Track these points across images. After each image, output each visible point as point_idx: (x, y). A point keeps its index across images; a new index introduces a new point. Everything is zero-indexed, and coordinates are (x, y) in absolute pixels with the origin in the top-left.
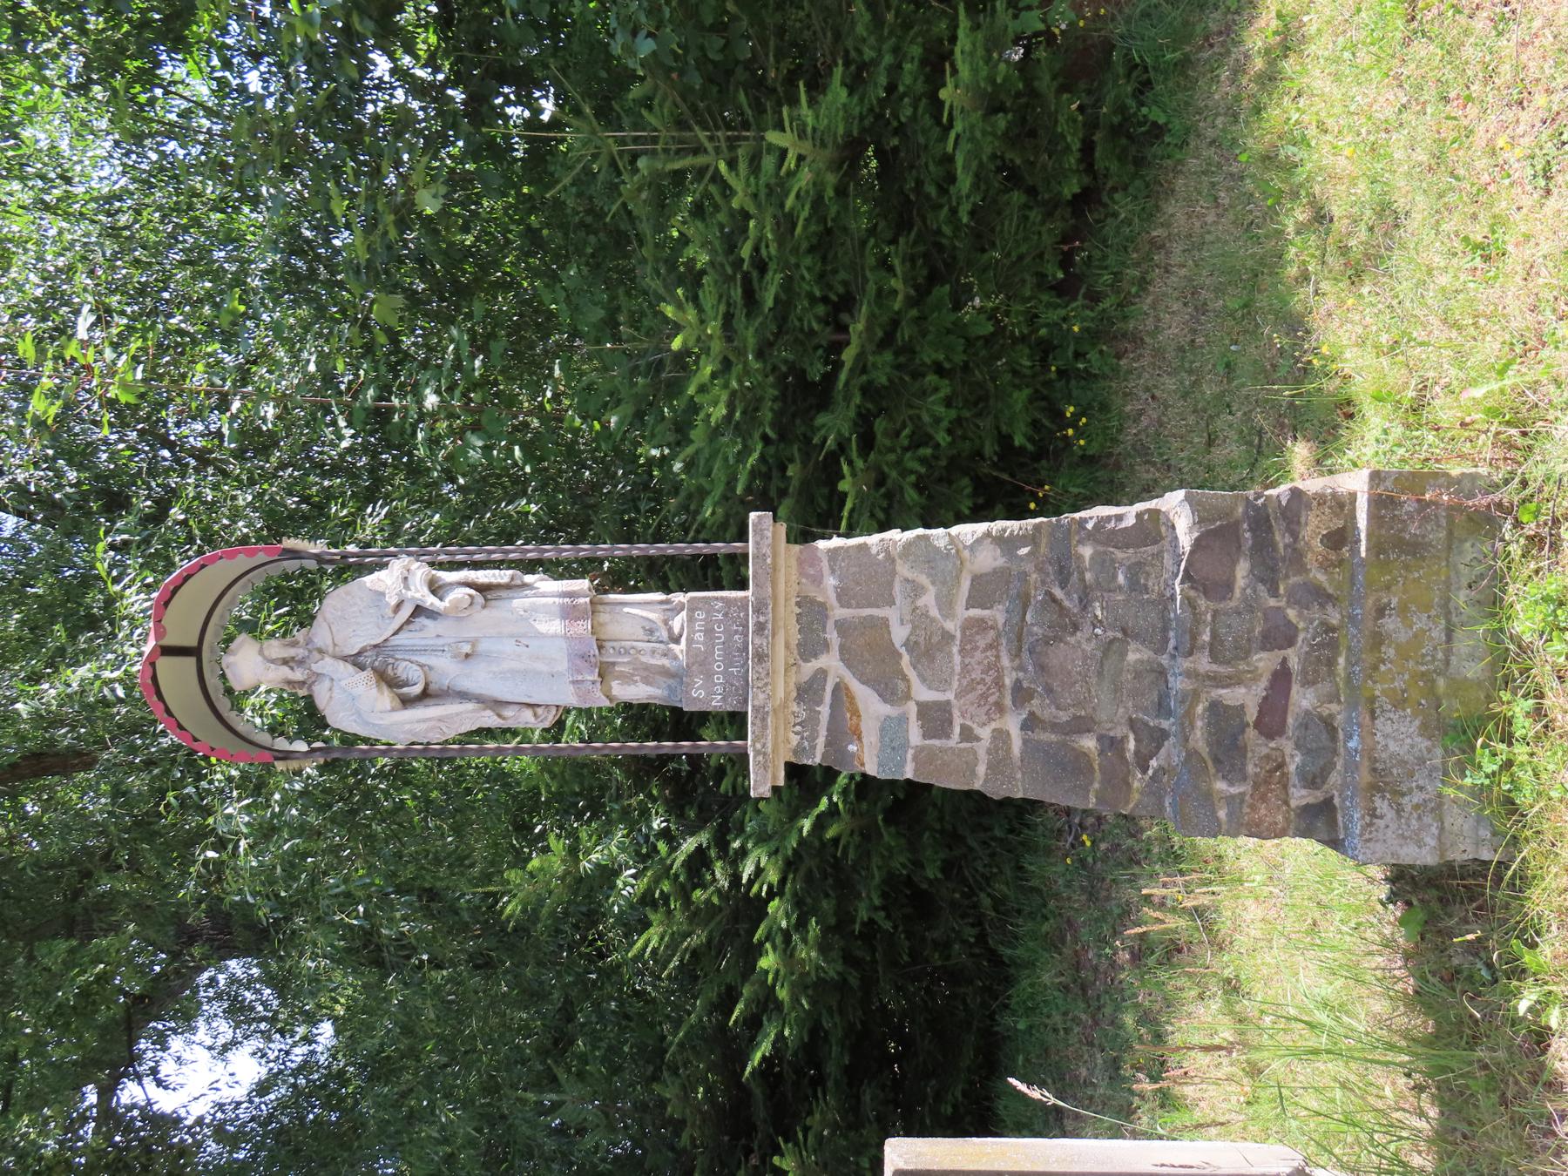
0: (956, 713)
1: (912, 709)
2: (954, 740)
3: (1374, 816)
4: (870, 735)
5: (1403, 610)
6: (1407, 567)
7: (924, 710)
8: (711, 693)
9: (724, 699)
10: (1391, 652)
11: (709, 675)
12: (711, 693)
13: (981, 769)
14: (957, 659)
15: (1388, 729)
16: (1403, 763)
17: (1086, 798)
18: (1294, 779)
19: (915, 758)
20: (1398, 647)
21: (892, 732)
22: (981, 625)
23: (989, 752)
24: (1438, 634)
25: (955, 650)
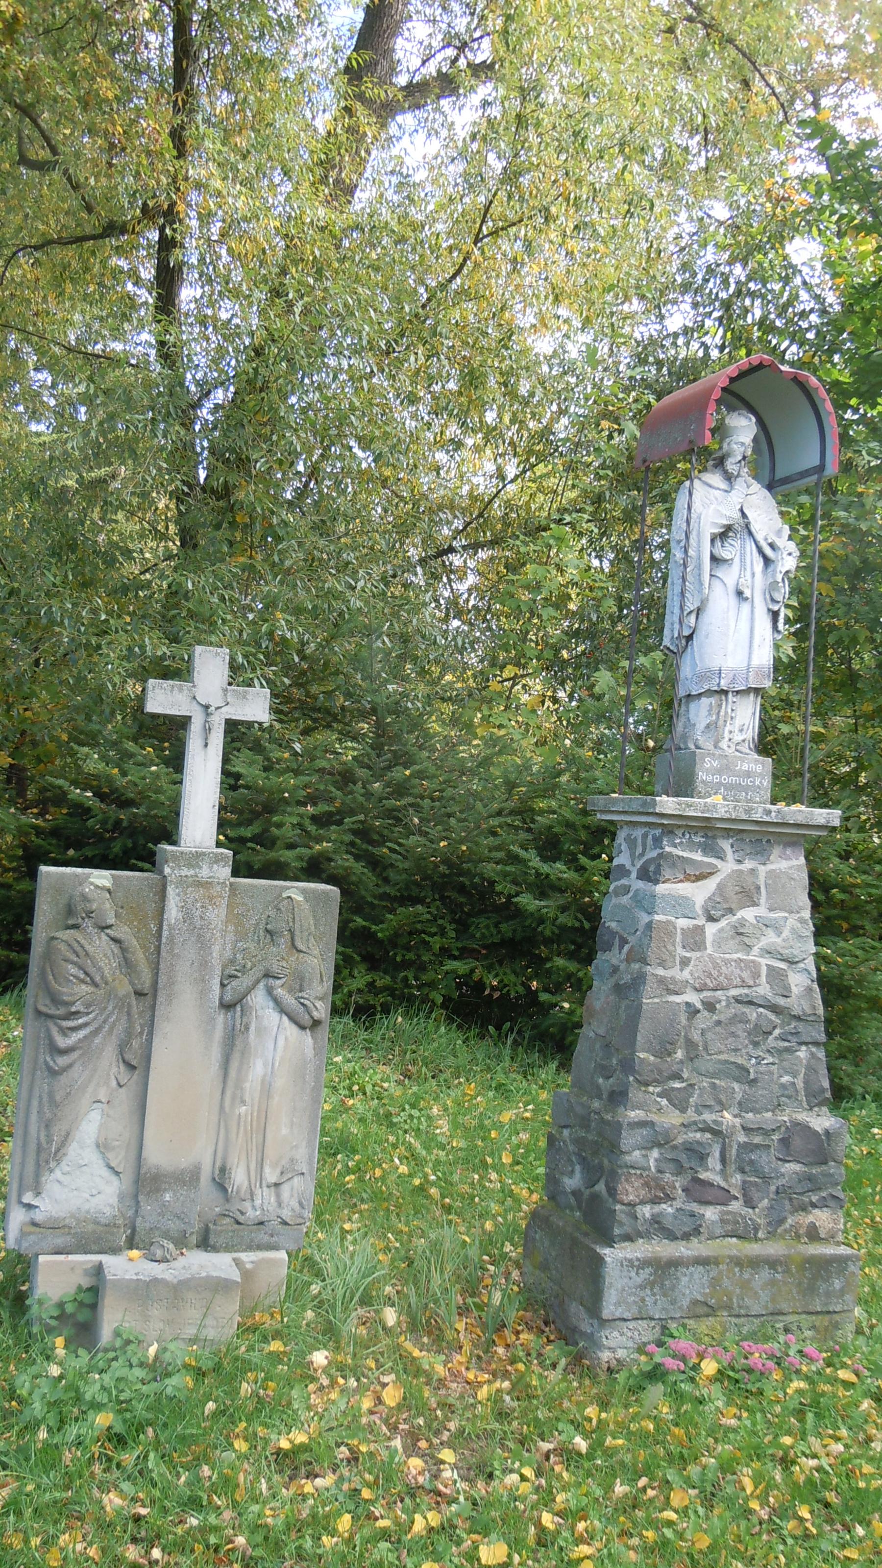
0: (698, 954)
1: (701, 921)
2: (680, 952)
3: (639, 1268)
4: (684, 889)
5: (773, 1283)
6: (800, 1284)
7: (700, 930)
8: (708, 771)
9: (703, 782)
10: (746, 1276)
11: (719, 772)
12: (708, 771)
13: (660, 972)
14: (735, 956)
15: (696, 1276)
16: (673, 1288)
17: (643, 1051)
18: (657, 1209)
19: (669, 922)
20: (749, 1281)
21: (682, 905)
22: (756, 975)
23: (673, 978)
24: (756, 1309)
25: (739, 955)
